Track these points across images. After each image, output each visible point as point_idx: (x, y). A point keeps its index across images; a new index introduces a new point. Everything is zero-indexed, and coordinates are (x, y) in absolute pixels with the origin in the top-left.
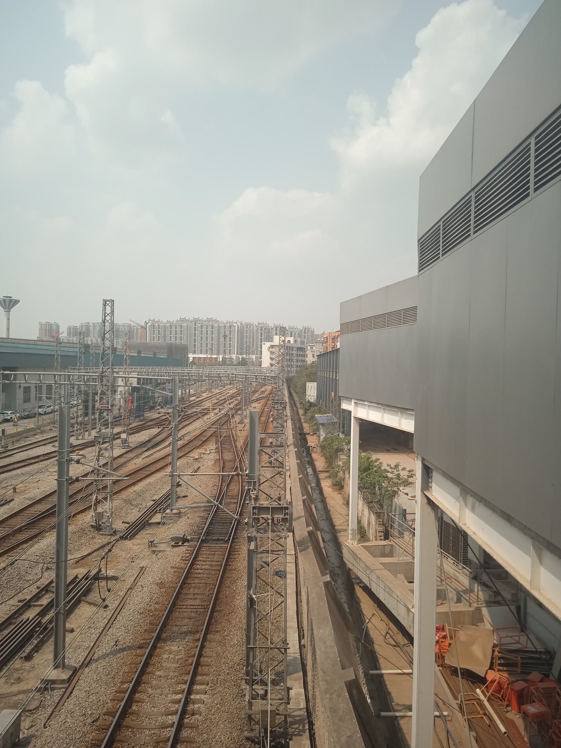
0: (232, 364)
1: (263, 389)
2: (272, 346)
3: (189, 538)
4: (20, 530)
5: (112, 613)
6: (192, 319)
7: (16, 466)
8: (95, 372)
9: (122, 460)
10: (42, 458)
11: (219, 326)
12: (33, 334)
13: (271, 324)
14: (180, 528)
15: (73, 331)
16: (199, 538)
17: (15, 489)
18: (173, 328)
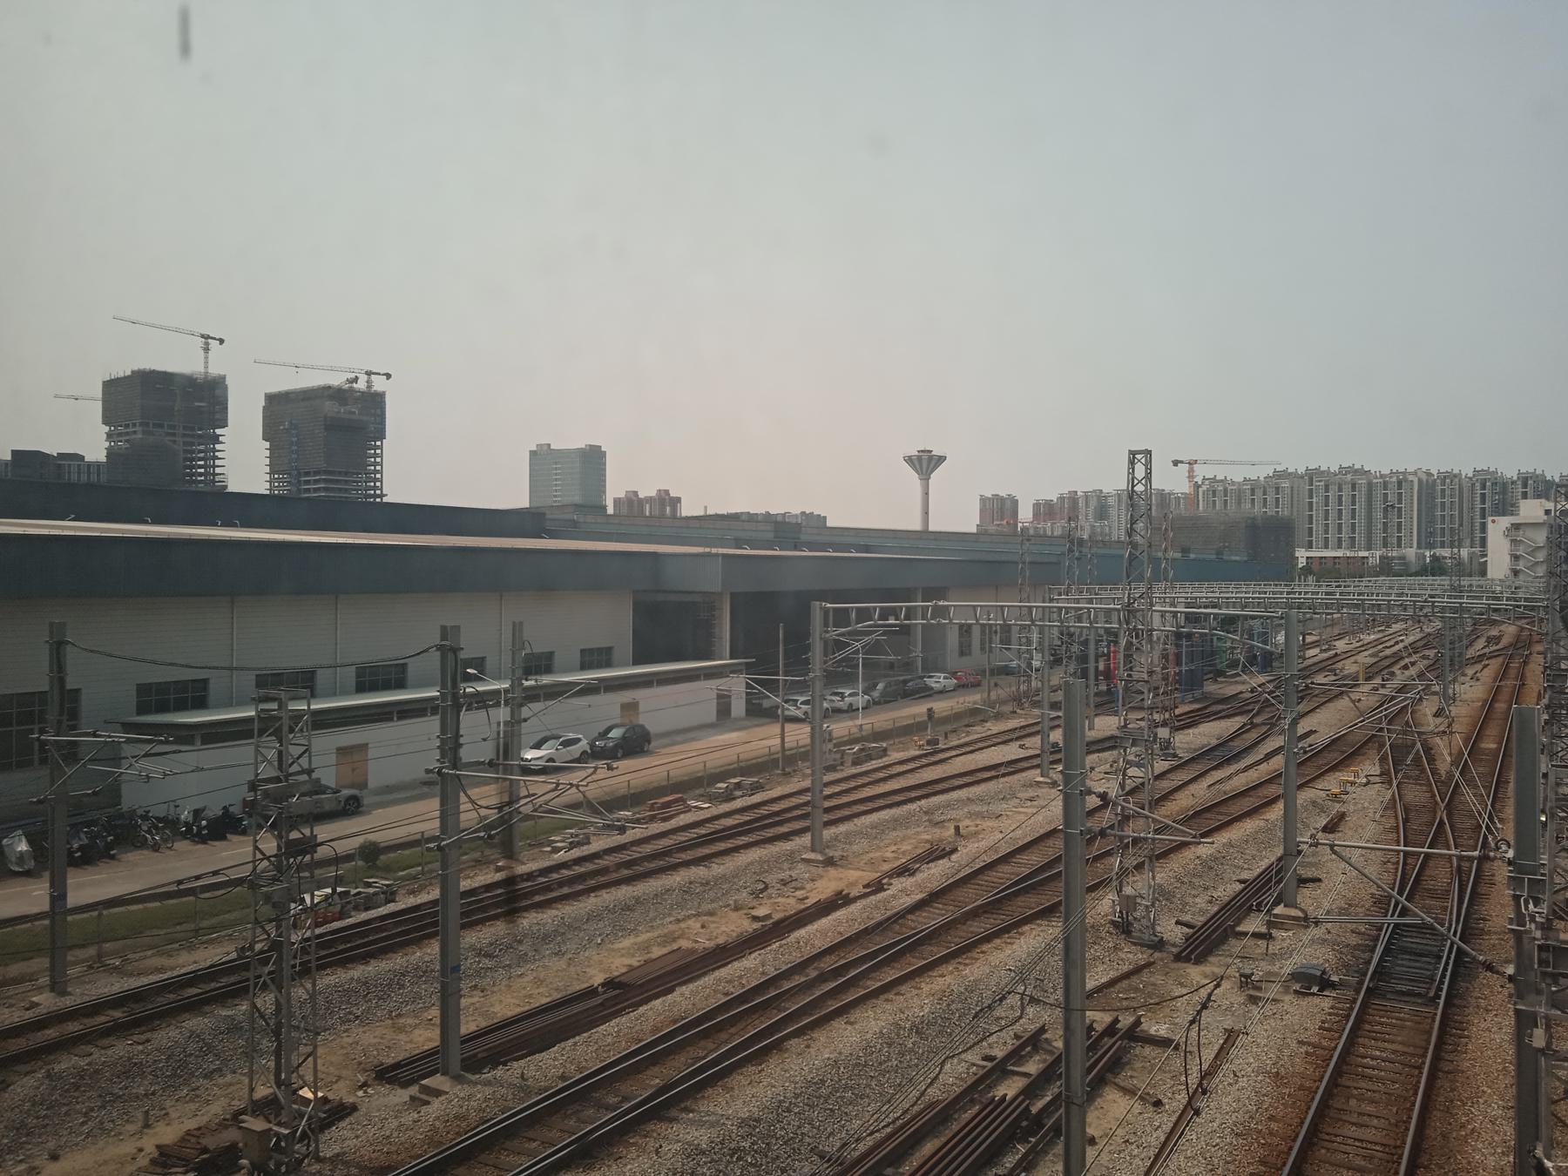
0: (1406, 572)
1: (1494, 632)
2: (1516, 527)
3: (1335, 978)
4: (975, 914)
5: (1174, 1119)
6: (1302, 470)
7: (957, 782)
8: (1112, 599)
9: (1166, 785)
10: (1003, 770)
11: (1370, 484)
12: (968, 522)
13: (1510, 473)
14: (1304, 950)
15: (1045, 510)
16: (1361, 983)
17: (957, 828)
18: (1259, 493)
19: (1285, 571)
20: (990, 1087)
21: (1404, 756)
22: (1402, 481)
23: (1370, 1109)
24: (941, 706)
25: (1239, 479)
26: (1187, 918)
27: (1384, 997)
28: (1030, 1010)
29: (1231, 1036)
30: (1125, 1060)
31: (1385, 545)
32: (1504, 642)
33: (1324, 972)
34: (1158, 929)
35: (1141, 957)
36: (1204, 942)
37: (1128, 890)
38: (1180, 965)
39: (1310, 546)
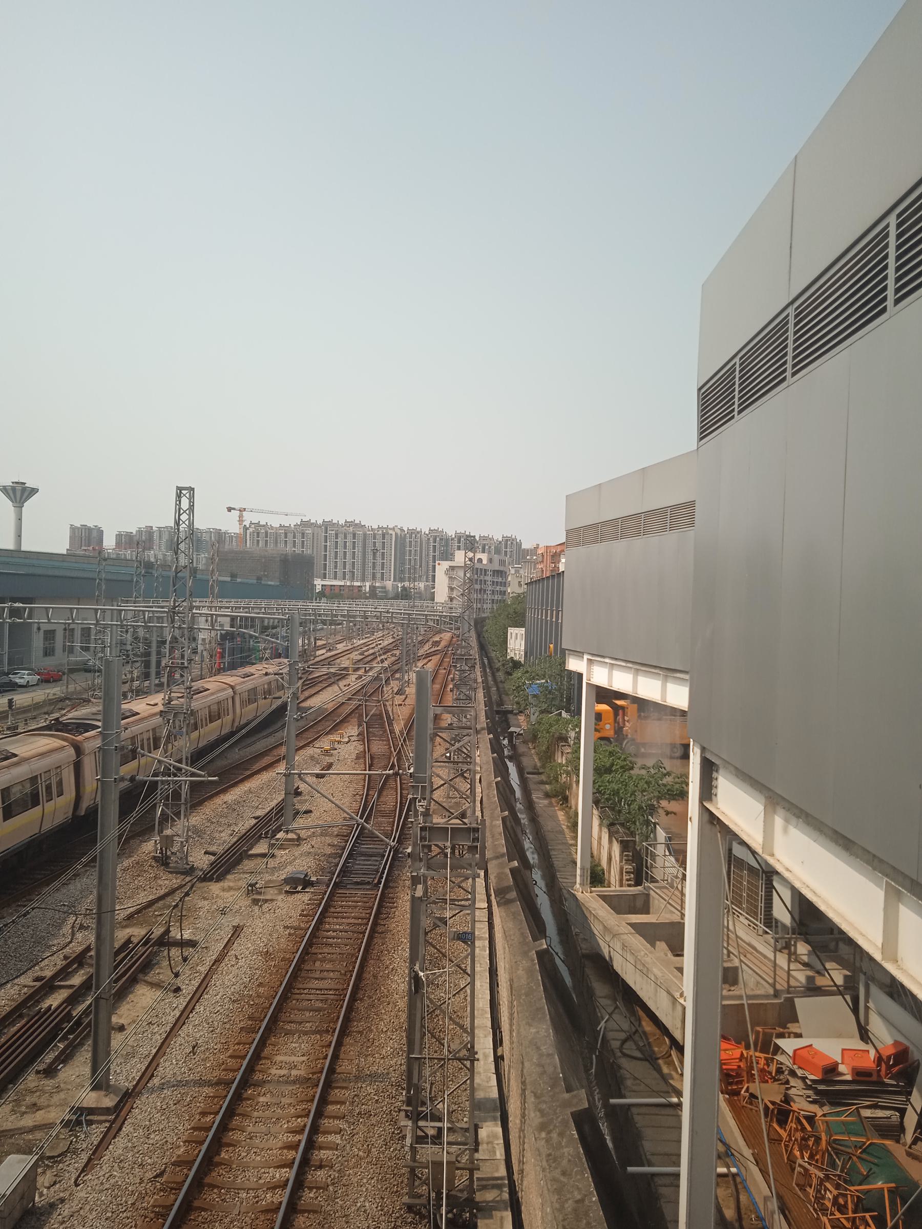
1: (437, 639)
3: (314, 879)
6: (320, 522)
11: (365, 535)
12: (60, 545)
13: (451, 533)
14: (298, 861)
15: (124, 540)
16: (331, 880)
19: (307, 592)
20: (38, 1002)
21: (375, 724)
22: (385, 533)
23: (329, 966)
24: (21, 699)
25: (276, 525)
26: (213, 849)
27: (345, 887)
28: (79, 936)
29: (237, 931)
30: (155, 962)
31: (374, 578)
32: (443, 644)
33: (306, 875)
34: (190, 859)
35: (176, 881)
36: (224, 866)
37: (168, 832)
38: (204, 884)
39: (324, 577)
